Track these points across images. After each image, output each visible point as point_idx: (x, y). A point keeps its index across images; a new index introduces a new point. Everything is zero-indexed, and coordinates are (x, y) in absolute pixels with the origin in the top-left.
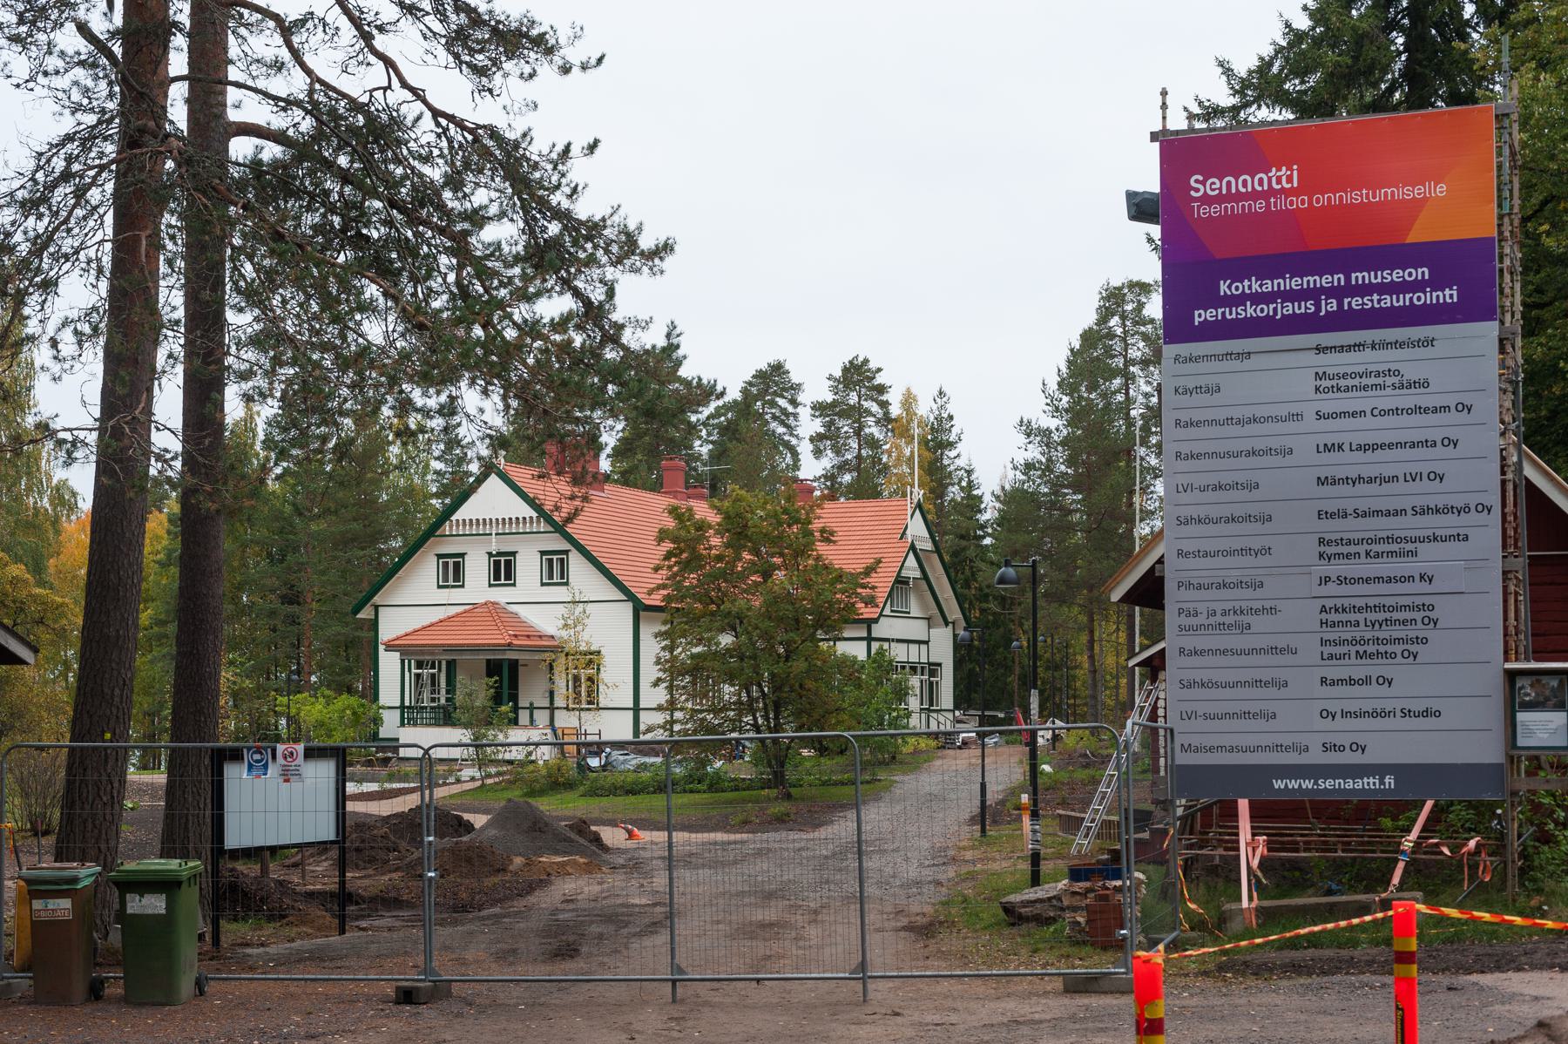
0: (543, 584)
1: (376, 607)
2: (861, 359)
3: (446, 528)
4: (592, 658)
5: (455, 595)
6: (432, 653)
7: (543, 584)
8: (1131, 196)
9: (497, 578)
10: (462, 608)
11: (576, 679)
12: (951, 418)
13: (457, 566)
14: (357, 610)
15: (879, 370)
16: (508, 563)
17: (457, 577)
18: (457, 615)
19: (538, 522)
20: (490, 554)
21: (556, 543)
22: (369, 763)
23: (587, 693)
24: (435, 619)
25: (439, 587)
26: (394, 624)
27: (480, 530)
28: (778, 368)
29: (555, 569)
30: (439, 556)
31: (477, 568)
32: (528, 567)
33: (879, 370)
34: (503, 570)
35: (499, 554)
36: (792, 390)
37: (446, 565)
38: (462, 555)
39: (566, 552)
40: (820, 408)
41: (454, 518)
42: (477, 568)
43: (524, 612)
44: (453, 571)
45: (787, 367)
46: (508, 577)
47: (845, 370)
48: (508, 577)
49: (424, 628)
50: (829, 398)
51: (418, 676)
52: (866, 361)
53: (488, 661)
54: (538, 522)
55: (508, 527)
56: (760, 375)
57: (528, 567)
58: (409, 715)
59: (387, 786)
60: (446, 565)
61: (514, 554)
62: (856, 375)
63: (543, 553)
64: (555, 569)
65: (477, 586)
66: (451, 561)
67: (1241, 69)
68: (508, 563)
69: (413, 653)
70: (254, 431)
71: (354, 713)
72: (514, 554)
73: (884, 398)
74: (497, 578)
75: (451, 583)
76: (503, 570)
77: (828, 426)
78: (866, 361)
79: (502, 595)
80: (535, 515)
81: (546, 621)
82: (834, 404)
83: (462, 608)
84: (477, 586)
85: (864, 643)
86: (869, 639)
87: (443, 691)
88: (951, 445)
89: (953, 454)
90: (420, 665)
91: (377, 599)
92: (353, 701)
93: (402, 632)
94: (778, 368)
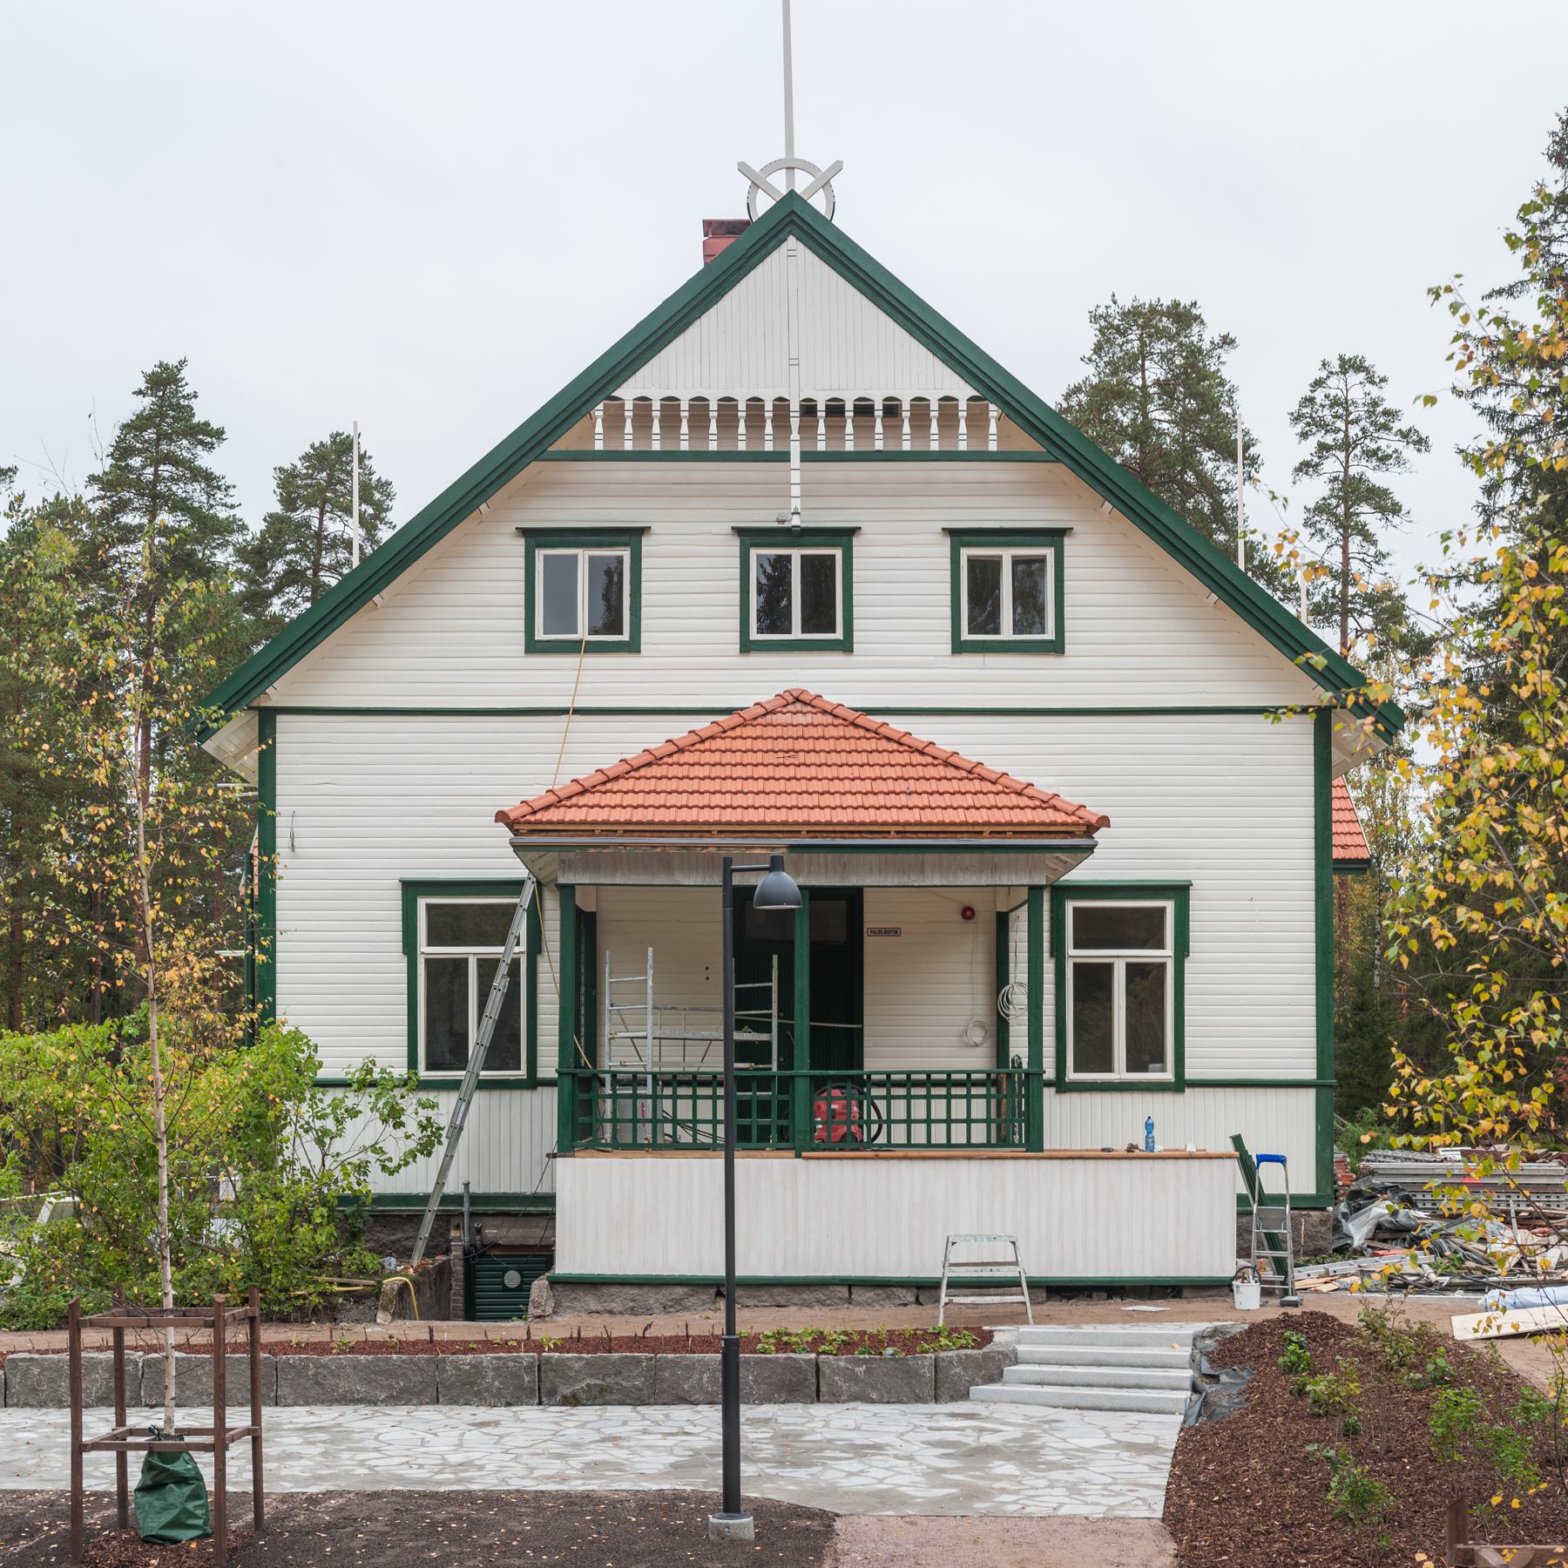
1: (267, 719)
4: (1143, 917)
5: (605, 679)
8: (708, 224)
9: (985, 618)
10: (702, 724)
11: (1093, 981)
16: (1028, 572)
17: (820, 613)
19: (977, 421)
24: (633, 752)
25: (533, 647)
27: (736, 431)
28: (223, 433)
30: (535, 537)
34: (800, 591)
38: (632, 536)
39: (1055, 536)
41: (628, 392)
44: (590, 592)
55: (850, 428)
60: (562, 576)
63: (959, 536)
67: (143, 386)
68: (1028, 572)
74: (985, 618)
76: (800, 591)
80: (963, 391)
83: (679, 729)
84: (693, 646)
91: (278, 693)
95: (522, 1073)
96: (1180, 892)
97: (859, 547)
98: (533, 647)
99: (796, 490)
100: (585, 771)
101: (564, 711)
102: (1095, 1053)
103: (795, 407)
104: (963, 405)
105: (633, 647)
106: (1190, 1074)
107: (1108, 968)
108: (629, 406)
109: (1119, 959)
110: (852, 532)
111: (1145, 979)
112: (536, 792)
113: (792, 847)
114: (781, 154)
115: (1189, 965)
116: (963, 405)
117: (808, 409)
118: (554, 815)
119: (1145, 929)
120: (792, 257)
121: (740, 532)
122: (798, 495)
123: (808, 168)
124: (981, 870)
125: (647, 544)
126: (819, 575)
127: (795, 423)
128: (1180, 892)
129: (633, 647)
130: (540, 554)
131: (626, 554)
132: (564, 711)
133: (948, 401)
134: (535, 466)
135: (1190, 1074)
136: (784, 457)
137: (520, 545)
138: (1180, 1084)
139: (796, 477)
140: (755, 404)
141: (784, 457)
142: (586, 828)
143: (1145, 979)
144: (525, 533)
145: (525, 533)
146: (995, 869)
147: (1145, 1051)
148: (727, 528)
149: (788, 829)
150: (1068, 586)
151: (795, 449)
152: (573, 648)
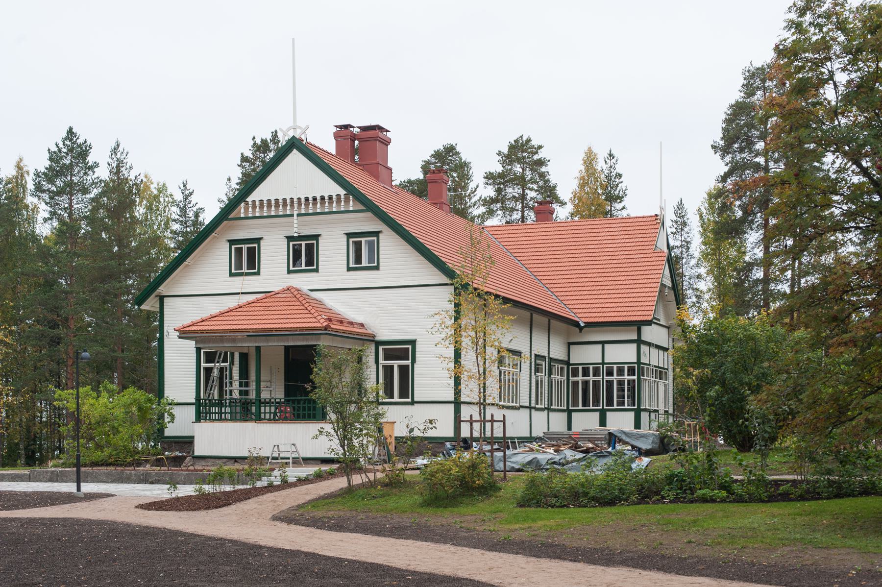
0: (349, 269)
1: (162, 298)
2: (525, 139)
3: (241, 210)
5: (251, 283)
6: (234, 340)
7: (349, 269)
10: (259, 296)
11: (389, 370)
12: (619, 176)
13: (251, 253)
14: (140, 301)
15: (540, 147)
16: (310, 248)
18: (258, 301)
19: (347, 200)
20: (290, 239)
21: (366, 223)
22: (159, 462)
23: (401, 384)
24: (224, 308)
25: (232, 275)
26: (178, 314)
27: (280, 209)
29: (361, 253)
30: (232, 242)
31: (274, 254)
32: (333, 251)
33: (540, 147)
34: (303, 253)
35: (301, 238)
36: (463, 169)
37: (239, 251)
38: (258, 240)
39: (377, 234)
40: (490, 177)
41: (249, 199)
42: (274, 254)
43: (331, 301)
44: (247, 257)
45: (458, 149)
46: (310, 262)
47: (512, 147)
48: (310, 262)
49: (222, 314)
50: (499, 169)
51: (208, 371)
52: (529, 140)
53: (287, 348)
54: (347, 200)
55: (312, 206)
56: (437, 155)
57: (333, 251)
58: (204, 410)
59: (207, 488)
60: (239, 251)
61: (316, 237)
62: (520, 152)
63: (349, 235)
64: (361, 253)
65: (274, 271)
66: (245, 247)
68: (310, 248)
69: (210, 344)
70: (24, 187)
71: (140, 409)
72: (316, 237)
73: (543, 169)
75: (245, 270)
76: (303, 253)
77: (499, 191)
78: (529, 140)
79: (304, 282)
80: (342, 192)
81: (352, 308)
82: (501, 175)
84: (274, 271)
85: (635, 346)
86: (639, 342)
87: (236, 385)
88: (620, 198)
89: (618, 206)
90: (210, 357)
91: (163, 289)
92: (140, 395)
93: (198, 318)
94: (450, 150)
95: (409, 400)
96: (413, 343)
97: (321, 240)
98: (232, 275)
99: (295, 226)
100: (206, 315)
101: (238, 294)
102: (389, 393)
103: (303, 200)
104: (343, 197)
105: (258, 273)
106: (416, 399)
107: (392, 366)
108: (250, 203)
109: (396, 364)
110: (319, 235)
111: (404, 370)
112: (188, 322)
113: (248, 336)
114: (292, 124)
115: (415, 366)
116: (343, 197)
117: (307, 199)
118: (187, 329)
119: (403, 355)
120: (296, 157)
121: (287, 237)
122: (296, 227)
123: (300, 128)
124: (303, 341)
125: (262, 242)
126: (310, 249)
127: (296, 205)
128: (413, 343)
129: (258, 273)
130: (233, 247)
131: (256, 245)
132: (238, 294)
133: (338, 196)
134: (225, 222)
135: (416, 399)
136: (292, 215)
137: (228, 244)
138: (413, 403)
139: (295, 221)
140: (285, 200)
141: (292, 215)
142: (202, 332)
143: (404, 370)
144: (229, 241)
145: (229, 241)
146: (307, 340)
147: (404, 393)
148: (283, 236)
149: (247, 330)
150: (381, 249)
151: (295, 213)
152: (241, 274)
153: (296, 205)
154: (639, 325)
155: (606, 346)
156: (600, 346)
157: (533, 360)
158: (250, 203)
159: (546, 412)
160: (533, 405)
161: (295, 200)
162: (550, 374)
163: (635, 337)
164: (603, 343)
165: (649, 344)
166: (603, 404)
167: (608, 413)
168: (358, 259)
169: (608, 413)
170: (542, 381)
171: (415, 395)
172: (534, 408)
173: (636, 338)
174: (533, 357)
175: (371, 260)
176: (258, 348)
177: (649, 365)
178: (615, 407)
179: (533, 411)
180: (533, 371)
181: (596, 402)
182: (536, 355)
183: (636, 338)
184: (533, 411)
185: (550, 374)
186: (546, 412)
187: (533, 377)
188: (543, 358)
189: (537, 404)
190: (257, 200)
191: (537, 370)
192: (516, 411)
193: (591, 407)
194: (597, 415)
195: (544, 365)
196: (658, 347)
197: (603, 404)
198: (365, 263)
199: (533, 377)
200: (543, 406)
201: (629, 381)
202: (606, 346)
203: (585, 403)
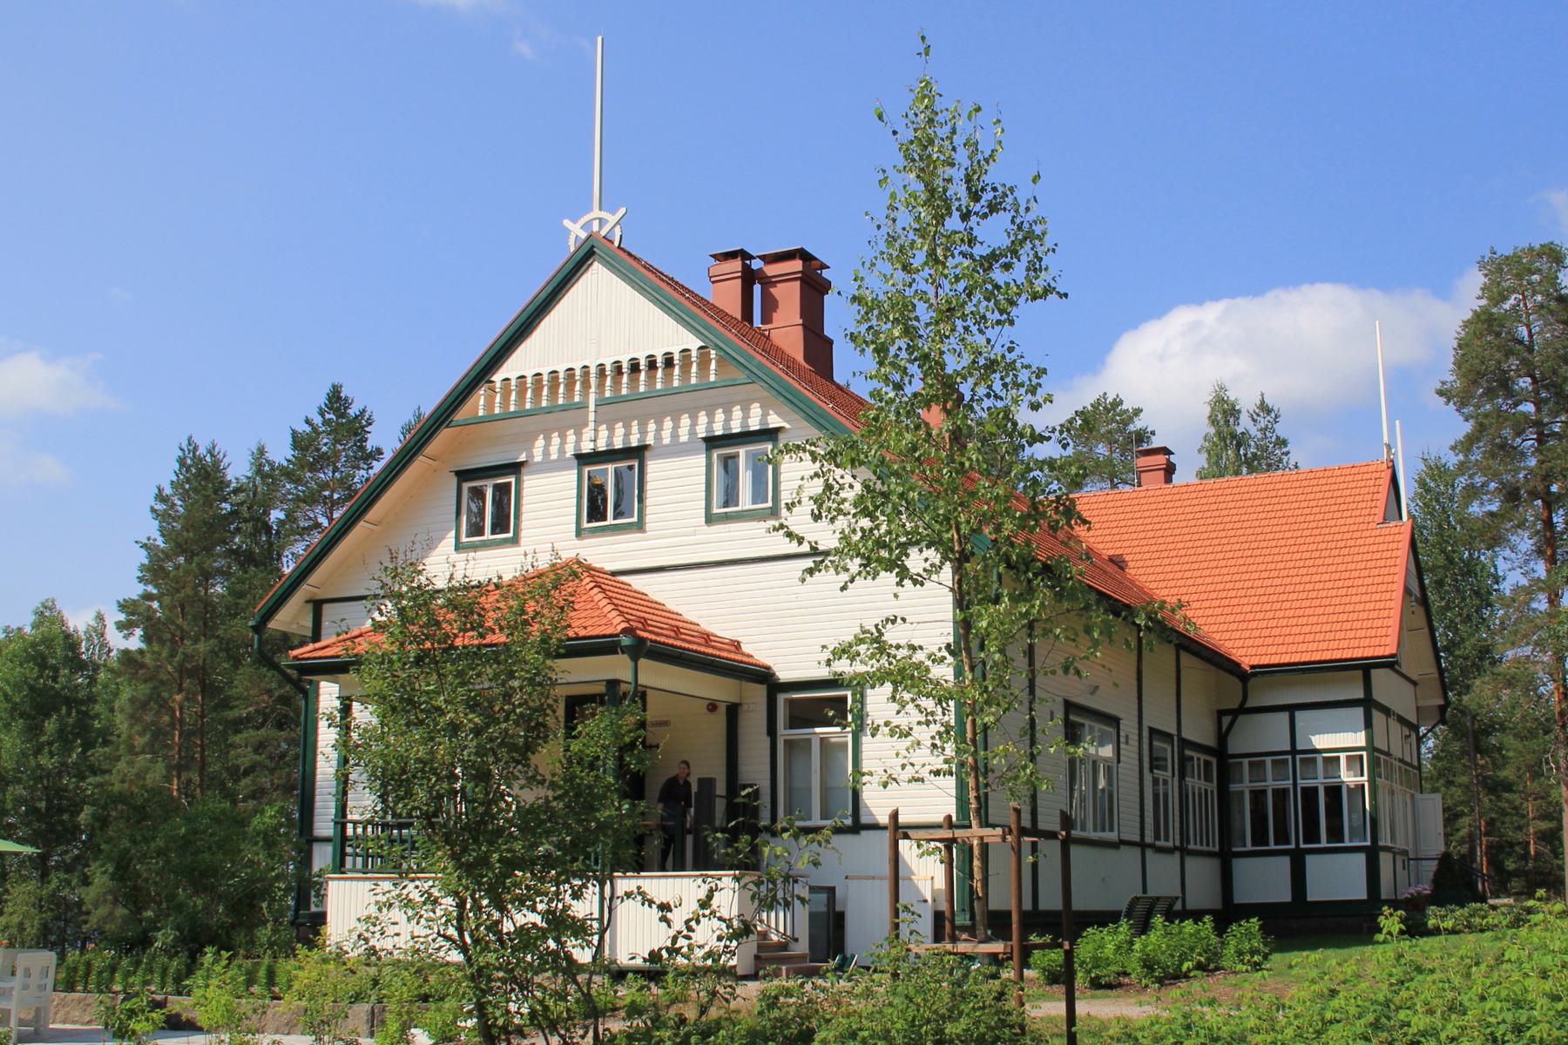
1: (317, 605)
3: (479, 402)
7: (710, 519)
27: (560, 396)
32: (676, 483)
41: (497, 378)
44: (490, 497)
79: (606, 552)
104: (694, 354)
108: (498, 385)
116: (694, 354)
137: (455, 480)
153: (593, 381)
154: (1365, 668)
155: (1299, 715)
156: (1285, 716)
157: (1146, 741)
158: (498, 385)
159: (1177, 855)
160: (1149, 839)
161: (593, 370)
162: (1182, 777)
163: (1359, 694)
164: (1292, 709)
165: (1386, 711)
166: (1296, 840)
167: (1309, 859)
168: (730, 497)
169: (1309, 859)
170: (1166, 795)
171: (1040, 818)
172: (1152, 846)
173: (1361, 695)
174: (1146, 734)
175: (758, 496)
176: (1103, 830)
177: (1388, 754)
178: (1324, 844)
179: (1149, 853)
180: (1146, 765)
181: (1282, 837)
182: (1152, 731)
183: (1361, 695)
184: (1149, 853)
185: (1182, 777)
186: (1177, 855)
187: (1148, 778)
188: (1166, 736)
189: (1157, 837)
190: (513, 376)
191: (1156, 762)
192: (1110, 854)
193: (1272, 847)
194: (1284, 863)
195: (1167, 750)
196: (1402, 720)
197: (1296, 840)
198: (745, 502)
199: (1148, 778)
200: (1170, 844)
201: (1275, 791)
202: (1299, 715)
203: (1260, 836)
